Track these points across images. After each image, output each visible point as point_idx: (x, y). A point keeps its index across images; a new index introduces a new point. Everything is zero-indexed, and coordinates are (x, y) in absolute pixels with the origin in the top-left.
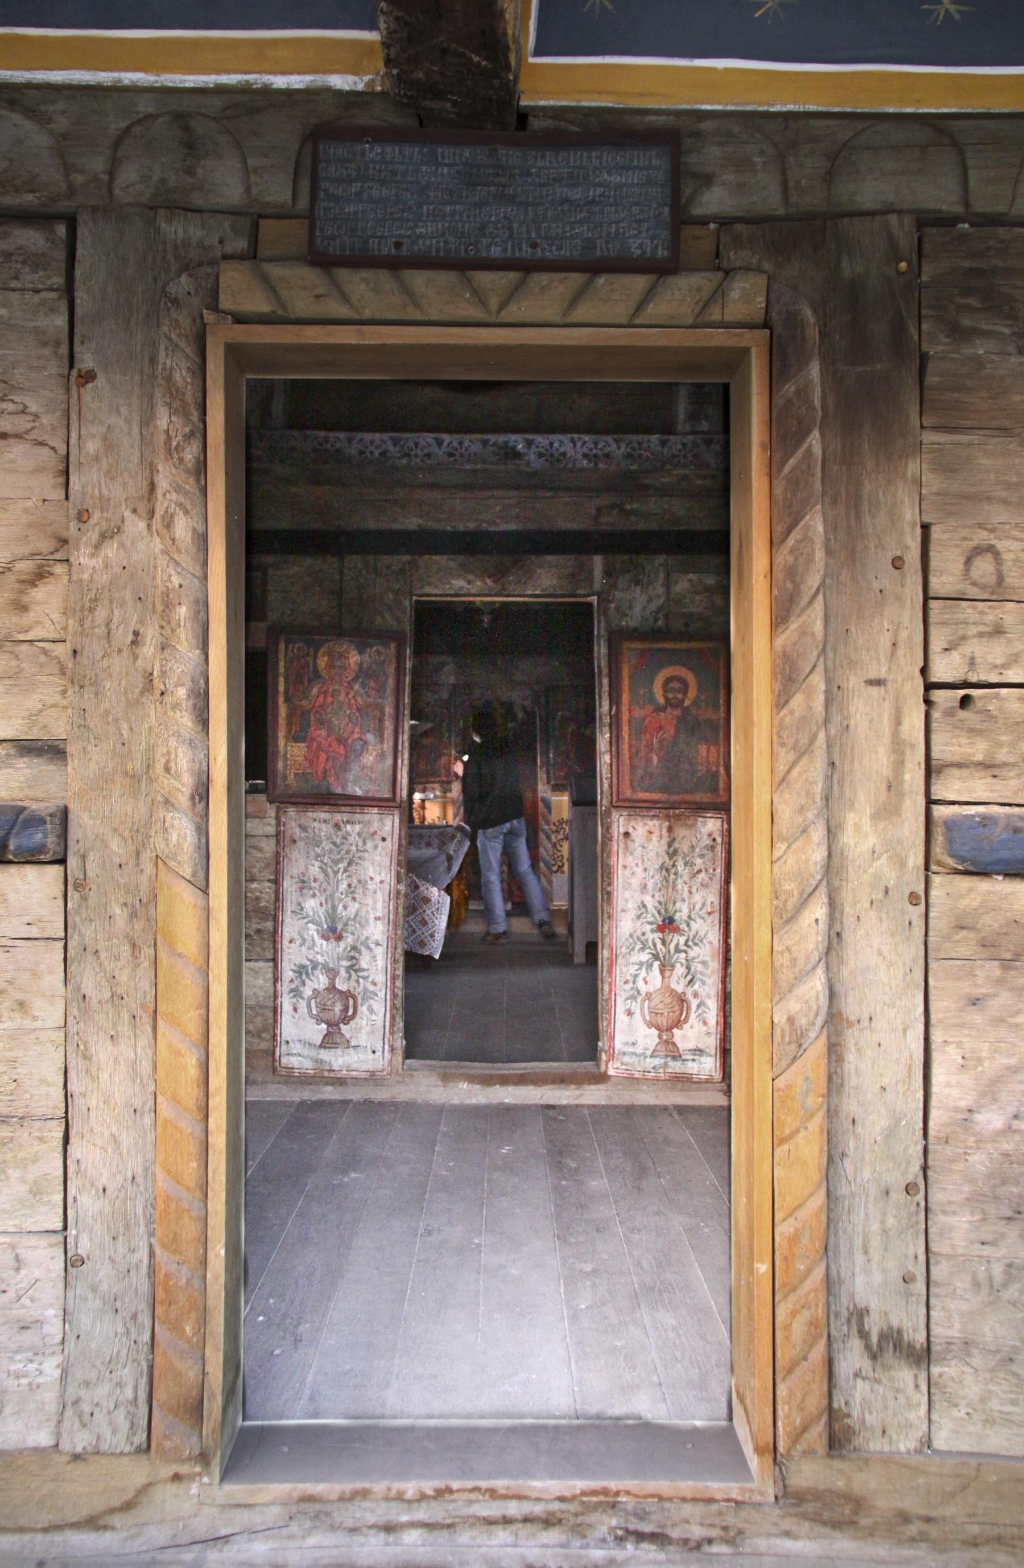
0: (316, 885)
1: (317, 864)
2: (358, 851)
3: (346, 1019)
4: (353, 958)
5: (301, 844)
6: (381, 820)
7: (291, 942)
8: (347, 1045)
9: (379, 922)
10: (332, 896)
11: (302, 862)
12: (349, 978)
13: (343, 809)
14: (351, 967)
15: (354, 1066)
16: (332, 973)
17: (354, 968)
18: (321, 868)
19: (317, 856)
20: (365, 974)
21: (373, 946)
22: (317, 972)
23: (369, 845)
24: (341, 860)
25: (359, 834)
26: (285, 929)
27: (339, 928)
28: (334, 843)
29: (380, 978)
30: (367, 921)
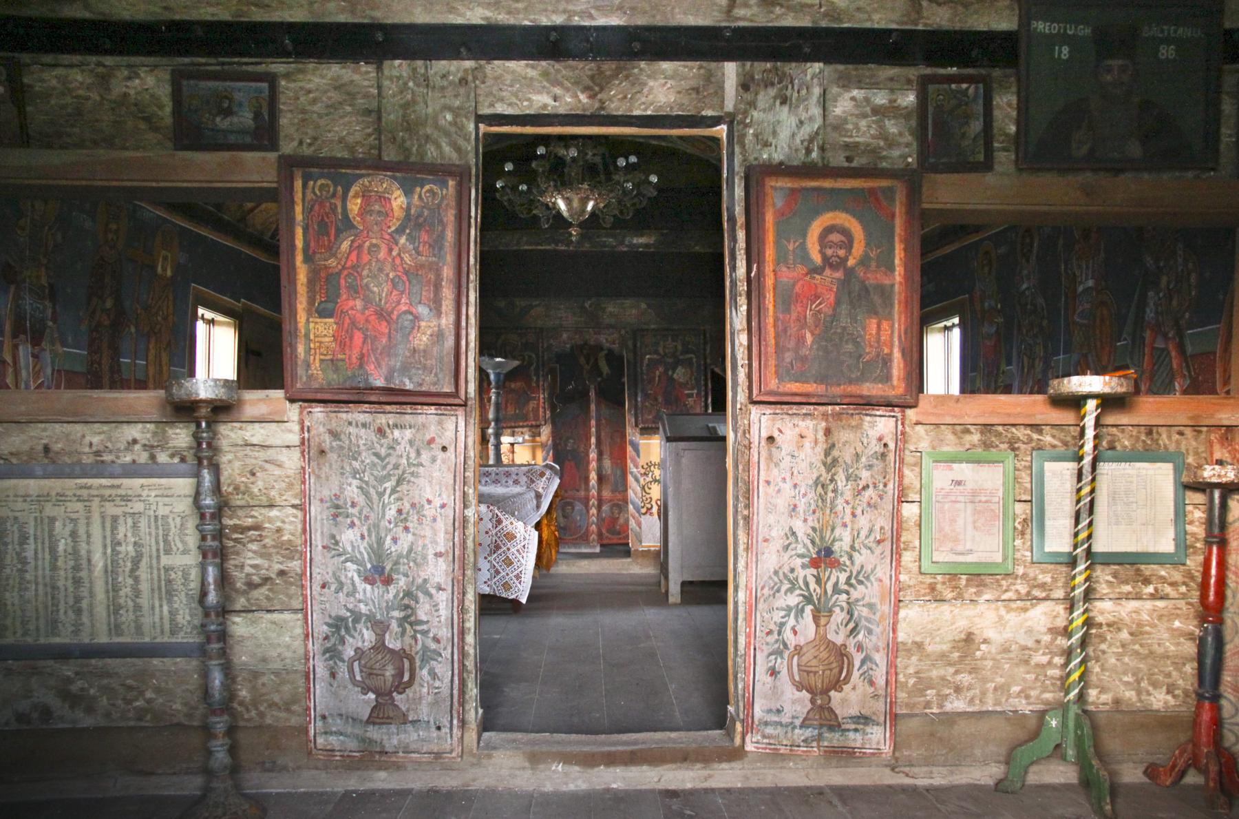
0: (355, 511)
1: (355, 482)
2: (409, 464)
3: (401, 687)
4: (407, 607)
5: (333, 456)
6: (440, 423)
7: (323, 586)
9: (441, 560)
10: (376, 526)
12: (403, 633)
14: (405, 618)
15: (413, 747)
16: (380, 627)
18: (360, 488)
19: (355, 473)
20: (425, 627)
21: (433, 591)
22: (359, 626)
23: (425, 457)
24: (387, 477)
25: (411, 442)
26: (316, 570)
27: (388, 568)
28: (377, 455)
30: (425, 557)
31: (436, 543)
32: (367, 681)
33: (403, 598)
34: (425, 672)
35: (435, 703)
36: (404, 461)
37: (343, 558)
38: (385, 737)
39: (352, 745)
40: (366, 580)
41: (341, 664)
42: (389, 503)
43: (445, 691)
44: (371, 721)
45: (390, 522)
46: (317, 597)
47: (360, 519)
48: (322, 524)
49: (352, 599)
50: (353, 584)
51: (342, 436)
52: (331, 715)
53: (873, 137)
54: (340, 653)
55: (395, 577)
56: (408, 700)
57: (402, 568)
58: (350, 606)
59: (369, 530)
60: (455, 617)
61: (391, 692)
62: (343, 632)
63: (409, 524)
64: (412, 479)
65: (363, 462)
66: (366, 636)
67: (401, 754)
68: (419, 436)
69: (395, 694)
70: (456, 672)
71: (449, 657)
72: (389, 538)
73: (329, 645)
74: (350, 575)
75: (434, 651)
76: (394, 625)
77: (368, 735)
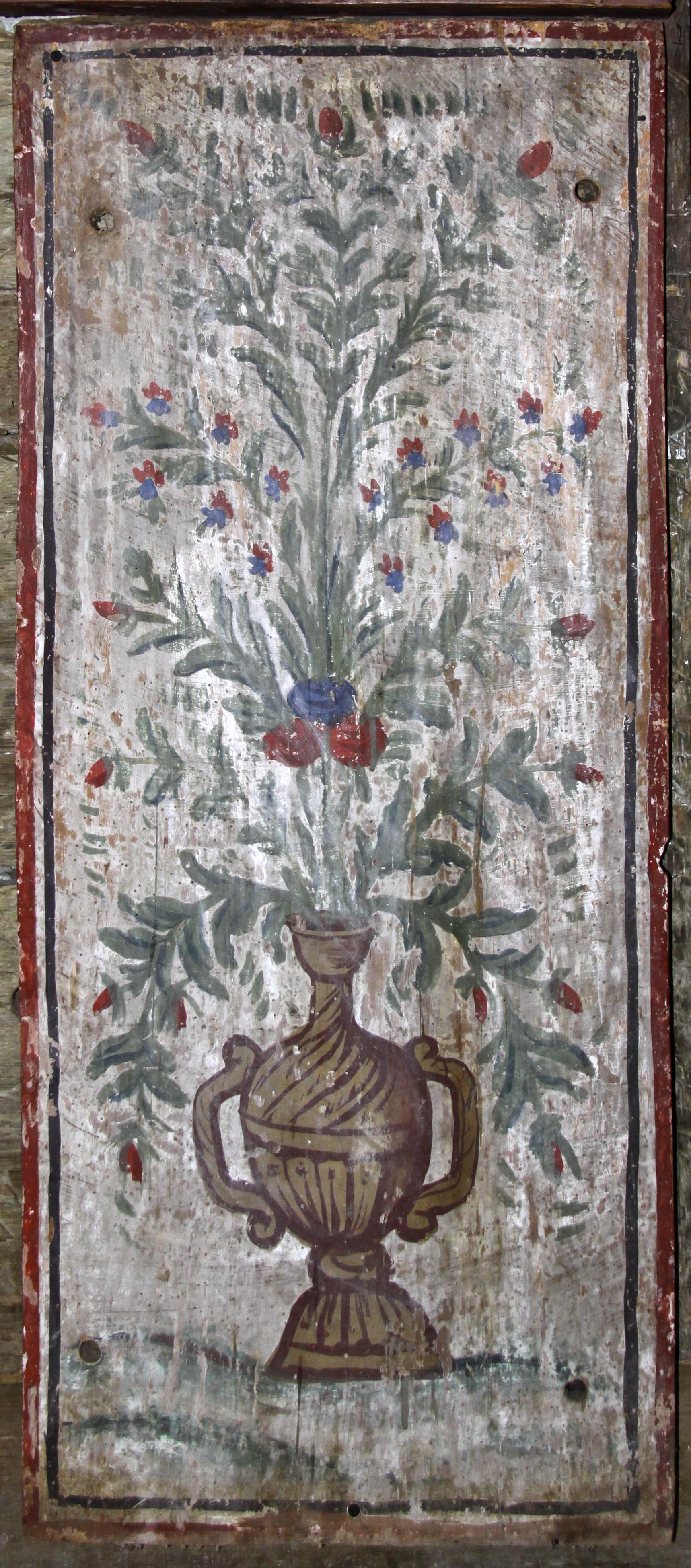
0: (230, 454)
1: (233, 336)
2: (452, 257)
3: (418, 1207)
4: (443, 854)
5: (142, 233)
6: (571, 88)
7: (98, 776)
8: (428, 1351)
9: (580, 650)
10: (318, 514)
11: (151, 330)
12: (428, 969)
13: (364, 32)
14: (434, 906)
15: (469, 1478)
16: (330, 946)
17: (451, 912)
18: (252, 357)
19: (232, 298)
20: (516, 941)
21: (550, 784)
22: (243, 944)
23: (511, 223)
24: (360, 313)
25: (455, 168)
26: (69, 707)
27: (364, 689)
28: (320, 221)
29: (597, 964)
30: (515, 640)
31: (560, 577)
32: (275, 1186)
33: (427, 816)
34: (517, 1139)
35: (564, 1276)
36: (429, 243)
37: (180, 654)
38: (351, 1438)
39: (209, 1473)
40: (276, 744)
41: (164, 1111)
42: (370, 418)
43: (604, 1222)
44: (289, 1365)
45: (371, 497)
46: (72, 821)
47: (250, 485)
48: (99, 514)
49: (215, 827)
50: (221, 762)
51: (183, 151)
52: (124, 1339)
53: (267, 994)
54: (164, 1062)
55: (393, 726)
56: (446, 1266)
57: (421, 690)
58: (209, 858)
59: (287, 533)
60: (642, 893)
61: (376, 1232)
62: (176, 972)
63: (455, 506)
64: (463, 316)
65: (263, 251)
66: (272, 987)
67: (416, 1515)
68: (484, 142)
69: (391, 1241)
70: (648, 1134)
71: (618, 1068)
72: (367, 562)
73: (115, 1030)
74: (207, 723)
75: (557, 1042)
76: (389, 935)
77: (278, 1426)
